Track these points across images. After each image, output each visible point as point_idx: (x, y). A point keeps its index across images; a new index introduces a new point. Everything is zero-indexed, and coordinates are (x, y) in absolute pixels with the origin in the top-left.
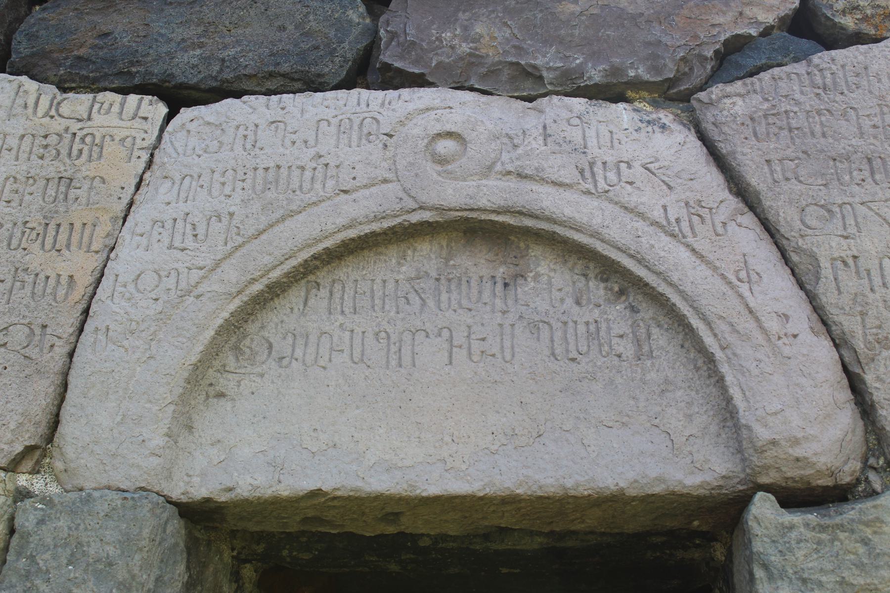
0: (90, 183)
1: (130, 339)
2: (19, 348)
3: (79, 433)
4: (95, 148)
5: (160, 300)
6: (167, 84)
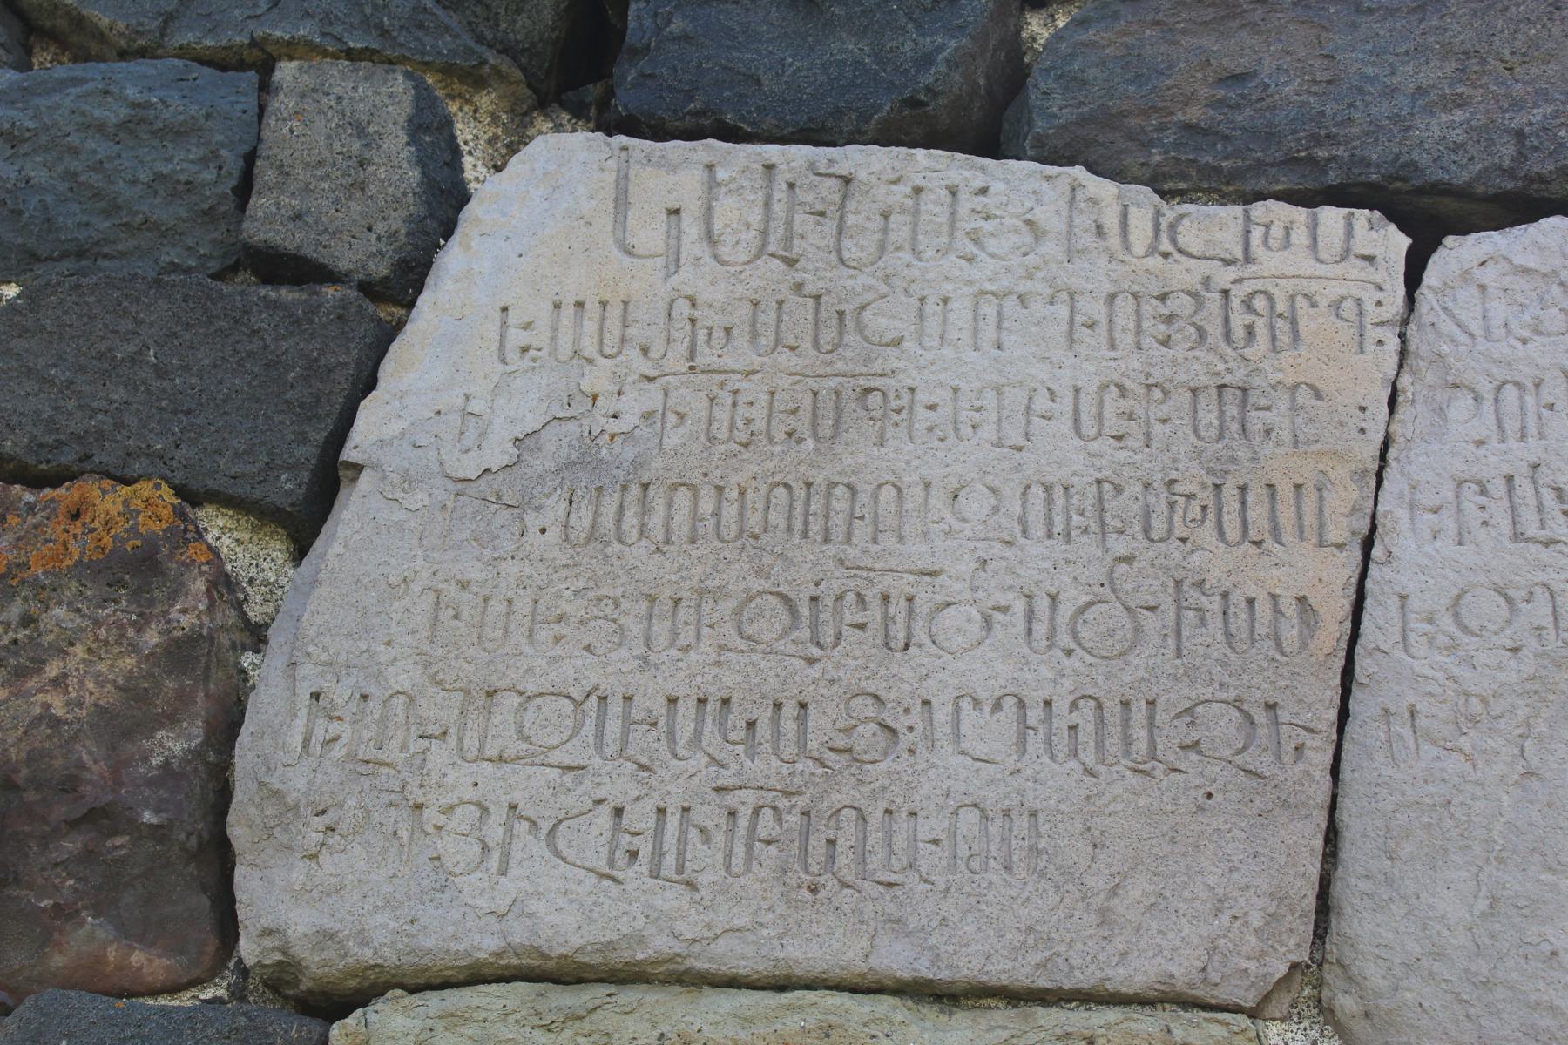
0: (1287, 397)
1: (1472, 733)
2: (1227, 752)
3: (1390, 935)
4: (1280, 323)
5: (1525, 651)
6: (1398, 184)
